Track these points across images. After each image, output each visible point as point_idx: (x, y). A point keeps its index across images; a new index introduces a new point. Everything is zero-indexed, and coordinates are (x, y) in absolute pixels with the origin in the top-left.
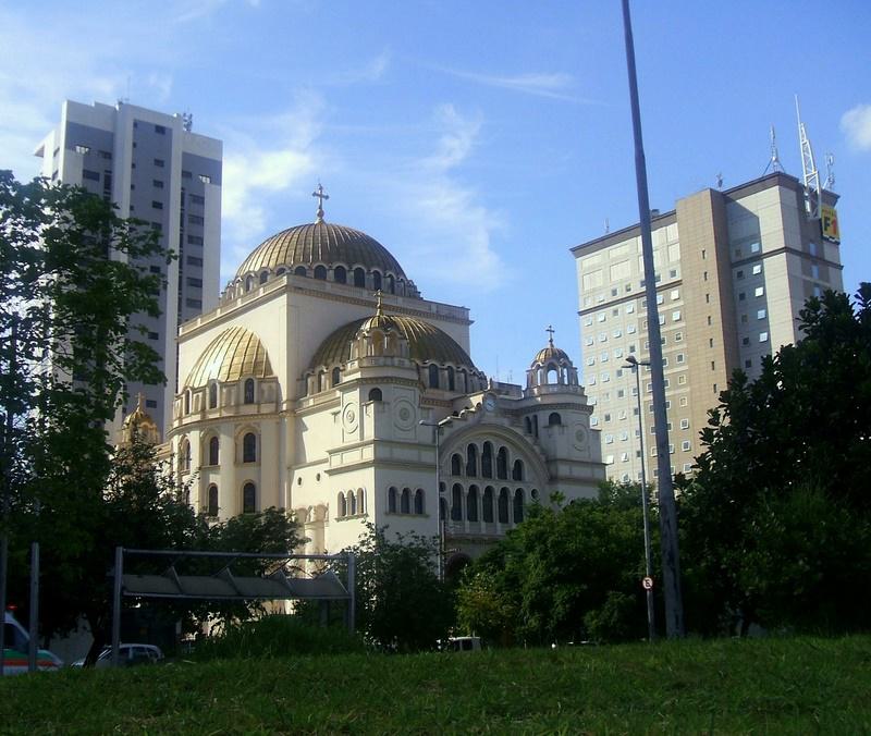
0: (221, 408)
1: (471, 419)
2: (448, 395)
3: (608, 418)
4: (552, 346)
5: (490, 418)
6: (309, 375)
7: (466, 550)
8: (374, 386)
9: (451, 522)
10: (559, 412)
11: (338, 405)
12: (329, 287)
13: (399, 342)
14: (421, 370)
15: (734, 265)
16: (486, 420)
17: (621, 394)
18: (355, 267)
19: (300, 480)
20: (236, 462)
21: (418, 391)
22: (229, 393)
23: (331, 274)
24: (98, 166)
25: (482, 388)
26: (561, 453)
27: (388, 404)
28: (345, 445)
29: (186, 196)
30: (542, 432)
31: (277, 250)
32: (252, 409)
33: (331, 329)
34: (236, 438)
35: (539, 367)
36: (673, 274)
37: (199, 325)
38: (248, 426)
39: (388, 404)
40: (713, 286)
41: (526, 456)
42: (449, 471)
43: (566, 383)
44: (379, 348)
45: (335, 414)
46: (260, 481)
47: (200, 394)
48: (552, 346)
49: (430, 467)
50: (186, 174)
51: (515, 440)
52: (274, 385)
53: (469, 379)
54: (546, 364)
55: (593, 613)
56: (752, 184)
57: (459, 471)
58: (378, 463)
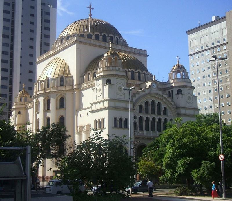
1: (147, 91)
3: (199, 94)
4: (179, 64)
5: (154, 91)
6: (84, 75)
7: (144, 142)
9: (139, 131)
10: (182, 89)
11: (94, 86)
12: (92, 42)
13: (118, 61)
14: (128, 73)
16: (152, 92)
17: (204, 85)
18: (103, 34)
19: (81, 115)
20: (57, 109)
21: (125, 80)
23: (93, 37)
25: (151, 80)
26: (182, 104)
30: (174, 96)
31: (73, 28)
32: (63, 88)
33: (95, 57)
34: (57, 99)
35: (173, 72)
36: (224, 40)
37: (44, 57)
38: (62, 94)
41: (167, 105)
42: (138, 111)
43: (184, 78)
44: (111, 64)
45: (93, 89)
46: (66, 116)
47: (43, 83)
48: (179, 64)
49: (126, 109)
50: (43, 4)
51: (162, 98)
52: (71, 79)
53: (146, 76)
54: (176, 71)
55: (196, 170)
58: (109, 108)
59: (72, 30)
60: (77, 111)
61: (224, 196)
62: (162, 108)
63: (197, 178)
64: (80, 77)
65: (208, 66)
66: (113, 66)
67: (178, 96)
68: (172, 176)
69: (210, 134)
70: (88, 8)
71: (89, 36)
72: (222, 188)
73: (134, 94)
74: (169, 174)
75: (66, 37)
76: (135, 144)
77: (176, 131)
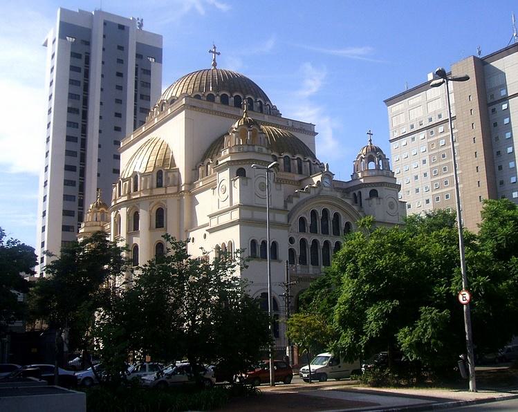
0: (141, 190)
1: (313, 192)
2: (297, 177)
4: (371, 144)
5: (327, 191)
8: (240, 166)
10: (378, 189)
15: (489, 105)
17: (417, 191)
20: (150, 229)
22: (146, 180)
23: (218, 99)
24: (81, 50)
27: (251, 179)
28: (220, 210)
29: (139, 69)
31: (182, 85)
32: (161, 191)
34: (150, 211)
39: (251, 179)
40: (476, 117)
43: (381, 168)
45: (214, 189)
47: (127, 182)
48: (371, 144)
50: (138, 56)
52: (176, 174)
54: (367, 156)
55: (406, 329)
56: (501, 52)
57: (305, 229)
58: (242, 222)
59: (180, 89)
60: (186, 231)
61: (473, 386)
62: (342, 223)
63: (410, 345)
64: (193, 170)
65: (424, 159)
66: (249, 145)
67: (370, 202)
68: (354, 345)
69: (440, 248)
70: (210, 51)
71: (211, 98)
72: (468, 369)
73: (289, 196)
74: (348, 340)
75: (169, 102)
76: (287, 286)
77: (362, 245)
